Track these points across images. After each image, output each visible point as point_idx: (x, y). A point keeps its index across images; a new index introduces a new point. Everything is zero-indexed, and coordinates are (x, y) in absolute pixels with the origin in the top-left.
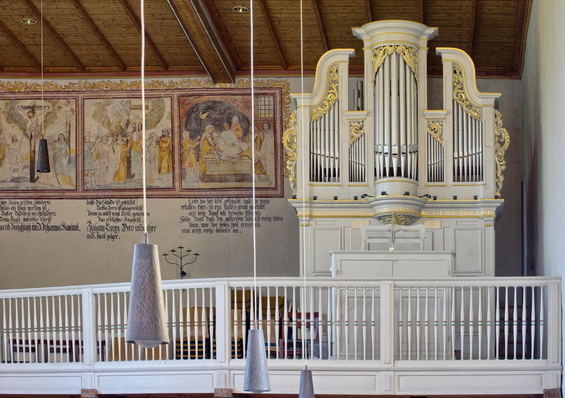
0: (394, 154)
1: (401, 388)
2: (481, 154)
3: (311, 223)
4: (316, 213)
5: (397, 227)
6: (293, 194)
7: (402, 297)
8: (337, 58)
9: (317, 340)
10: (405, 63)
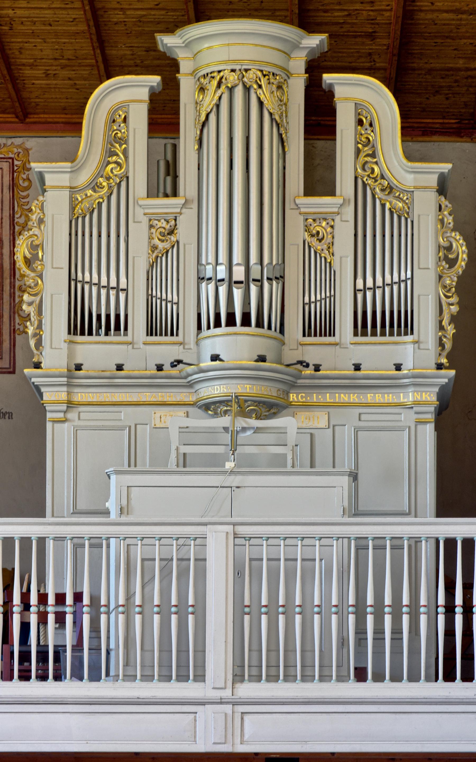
0: (236, 282)
1: (246, 737)
2: (409, 282)
3: (69, 416)
4: (80, 396)
5: (241, 422)
6: (35, 360)
7: (251, 560)
8: (125, 96)
9: (78, 646)
10: (261, 104)
